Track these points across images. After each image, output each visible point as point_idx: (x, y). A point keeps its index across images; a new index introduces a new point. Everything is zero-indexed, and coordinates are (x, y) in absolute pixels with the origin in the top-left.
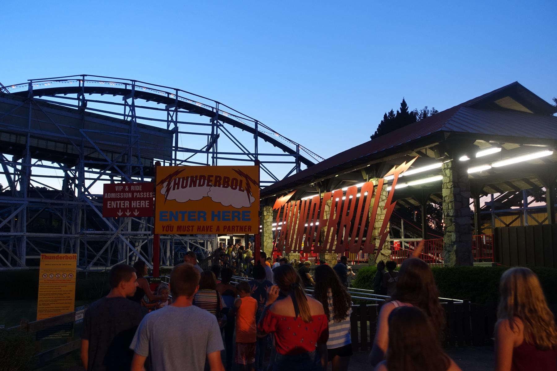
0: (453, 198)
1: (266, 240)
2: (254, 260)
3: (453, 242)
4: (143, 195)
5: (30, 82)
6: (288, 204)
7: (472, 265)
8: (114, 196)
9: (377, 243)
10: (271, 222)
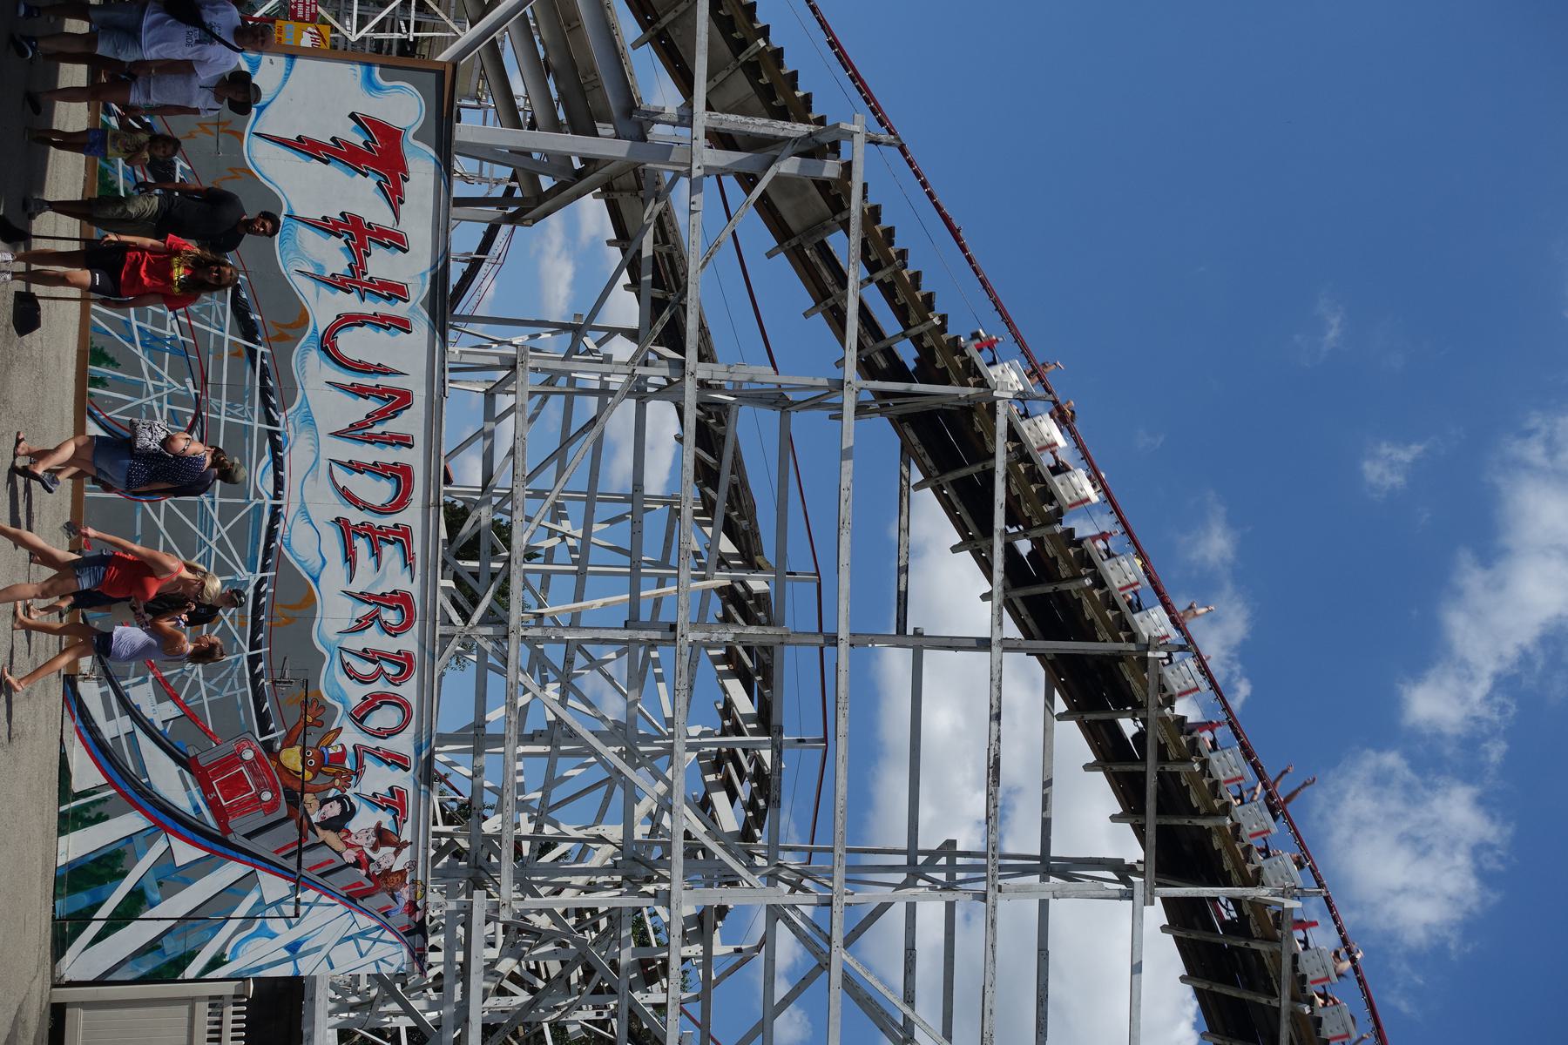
5: (361, 545)
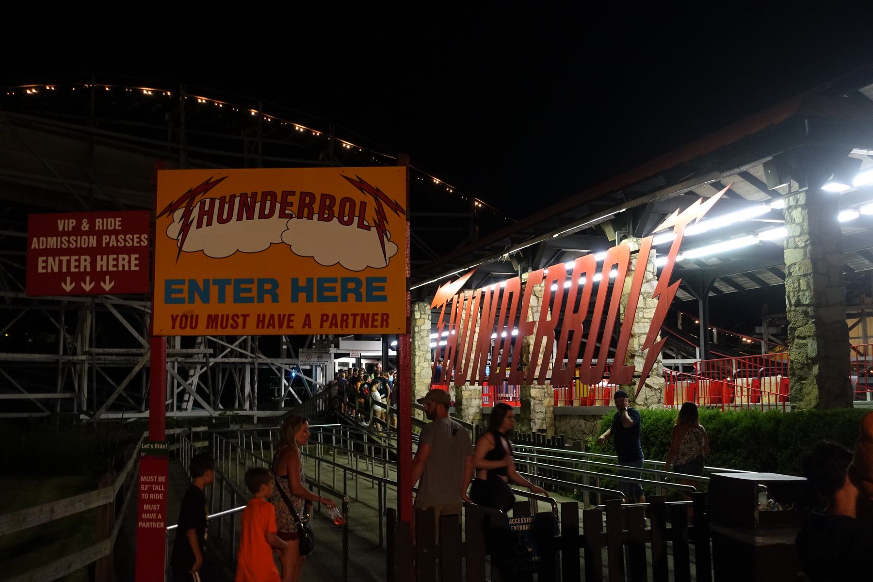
0: (810, 266)
1: (419, 363)
2: (396, 408)
3: (811, 359)
4: (125, 240)
6: (459, 297)
7: (851, 405)
8: (55, 244)
9: (639, 365)
10: (428, 331)
